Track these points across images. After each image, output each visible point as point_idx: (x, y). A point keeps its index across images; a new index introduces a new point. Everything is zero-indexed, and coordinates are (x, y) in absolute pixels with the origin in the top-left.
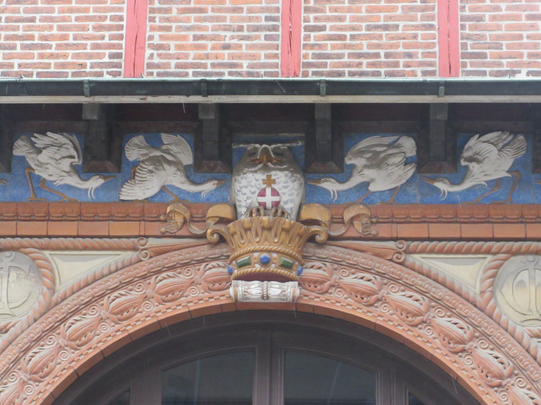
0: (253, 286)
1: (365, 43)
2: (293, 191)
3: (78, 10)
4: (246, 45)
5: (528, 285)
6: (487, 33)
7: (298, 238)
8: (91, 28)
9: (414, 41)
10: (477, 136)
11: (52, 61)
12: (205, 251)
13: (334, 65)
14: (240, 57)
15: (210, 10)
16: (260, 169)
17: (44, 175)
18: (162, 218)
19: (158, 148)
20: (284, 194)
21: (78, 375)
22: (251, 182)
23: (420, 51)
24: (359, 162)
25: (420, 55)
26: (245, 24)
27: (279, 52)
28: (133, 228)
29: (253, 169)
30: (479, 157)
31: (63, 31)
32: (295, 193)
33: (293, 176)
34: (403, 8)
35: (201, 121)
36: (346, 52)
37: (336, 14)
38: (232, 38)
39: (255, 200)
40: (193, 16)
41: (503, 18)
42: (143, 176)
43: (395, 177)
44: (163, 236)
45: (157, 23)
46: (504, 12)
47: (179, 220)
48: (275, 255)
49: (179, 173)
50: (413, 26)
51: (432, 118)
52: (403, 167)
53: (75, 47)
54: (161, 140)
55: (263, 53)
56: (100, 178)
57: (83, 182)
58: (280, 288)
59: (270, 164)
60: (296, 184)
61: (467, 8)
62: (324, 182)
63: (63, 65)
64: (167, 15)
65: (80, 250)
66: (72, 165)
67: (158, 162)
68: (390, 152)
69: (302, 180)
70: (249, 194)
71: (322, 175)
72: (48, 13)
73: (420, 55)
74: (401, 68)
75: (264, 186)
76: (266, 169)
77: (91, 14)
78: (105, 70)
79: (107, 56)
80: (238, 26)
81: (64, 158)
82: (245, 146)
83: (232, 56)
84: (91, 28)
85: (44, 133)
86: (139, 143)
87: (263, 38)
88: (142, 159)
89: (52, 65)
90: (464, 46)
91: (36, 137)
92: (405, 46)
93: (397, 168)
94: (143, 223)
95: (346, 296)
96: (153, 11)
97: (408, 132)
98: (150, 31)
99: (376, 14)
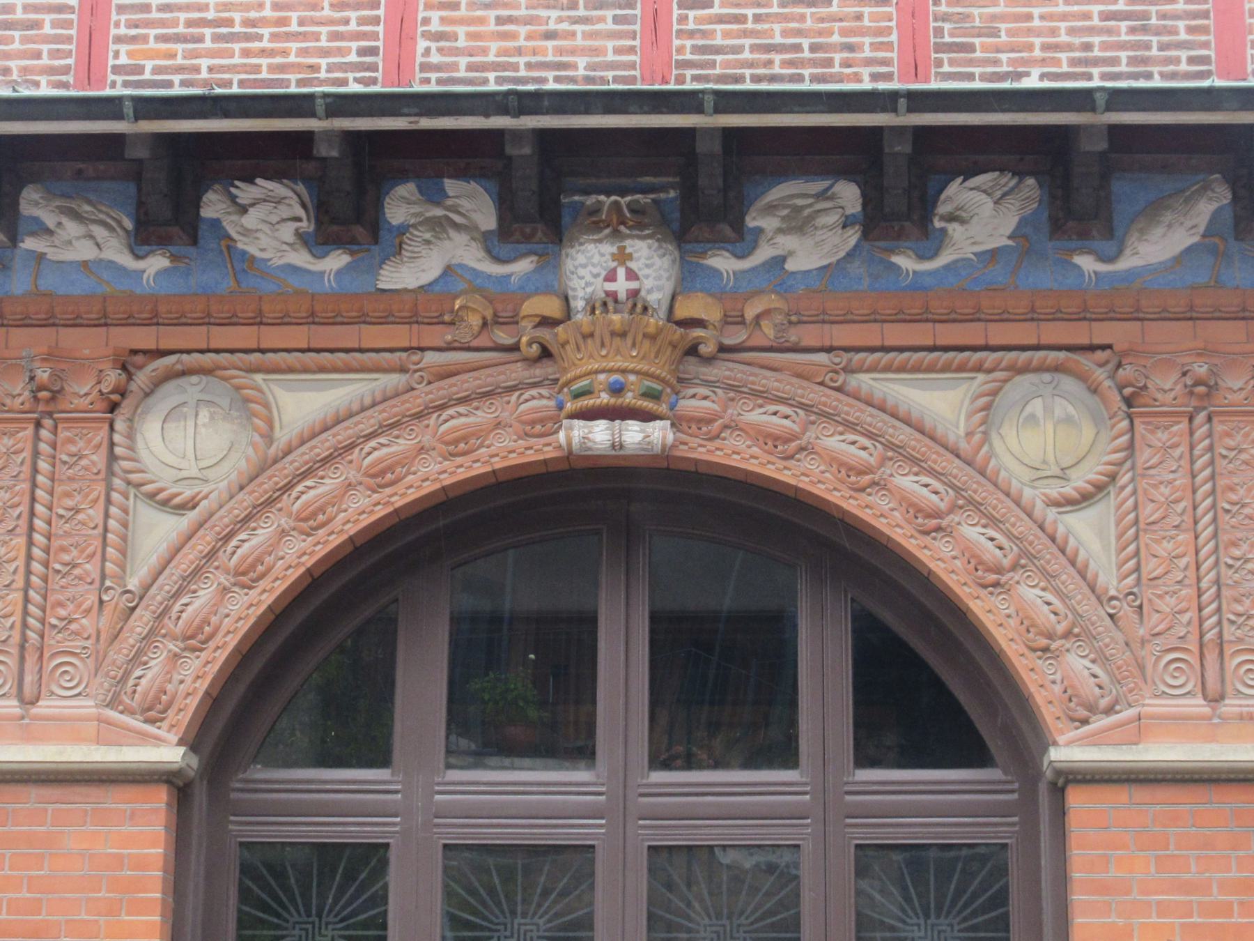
1: (777, 27)
2: (662, 272)
4: (584, 33)
5: (1042, 421)
7: (670, 349)
9: (858, 24)
10: (960, 179)
11: (264, 62)
12: (518, 372)
13: (726, 64)
14: (573, 52)
16: (607, 237)
17: (253, 250)
18: (447, 318)
19: (438, 204)
20: (647, 277)
21: (311, 575)
22: (592, 257)
23: (867, 40)
24: (769, 223)
25: (867, 48)
27: (637, 43)
28: (400, 335)
30: (964, 214)
31: (281, 11)
32: (665, 275)
33: (660, 247)
35: (510, 158)
36: (747, 42)
38: (560, 20)
39: (599, 287)
42: (416, 249)
44: (449, 348)
47: (475, 321)
48: (632, 378)
49: (474, 244)
52: (840, 231)
55: (610, 45)
56: (345, 253)
57: (316, 261)
58: (642, 431)
59: (622, 228)
60: (666, 261)
62: (711, 257)
63: (282, 68)
65: (314, 372)
66: (297, 233)
67: (440, 226)
69: (677, 253)
70: (589, 278)
73: (867, 48)
75: (615, 264)
76: (616, 235)
78: (351, 76)
81: (284, 220)
83: (560, 51)
85: (250, 180)
87: (610, 20)
88: (412, 221)
89: (264, 68)
90: (939, 32)
91: (237, 187)
92: (844, 32)
93: (830, 233)
94: (415, 326)
95: (749, 443)
97: (846, 173)
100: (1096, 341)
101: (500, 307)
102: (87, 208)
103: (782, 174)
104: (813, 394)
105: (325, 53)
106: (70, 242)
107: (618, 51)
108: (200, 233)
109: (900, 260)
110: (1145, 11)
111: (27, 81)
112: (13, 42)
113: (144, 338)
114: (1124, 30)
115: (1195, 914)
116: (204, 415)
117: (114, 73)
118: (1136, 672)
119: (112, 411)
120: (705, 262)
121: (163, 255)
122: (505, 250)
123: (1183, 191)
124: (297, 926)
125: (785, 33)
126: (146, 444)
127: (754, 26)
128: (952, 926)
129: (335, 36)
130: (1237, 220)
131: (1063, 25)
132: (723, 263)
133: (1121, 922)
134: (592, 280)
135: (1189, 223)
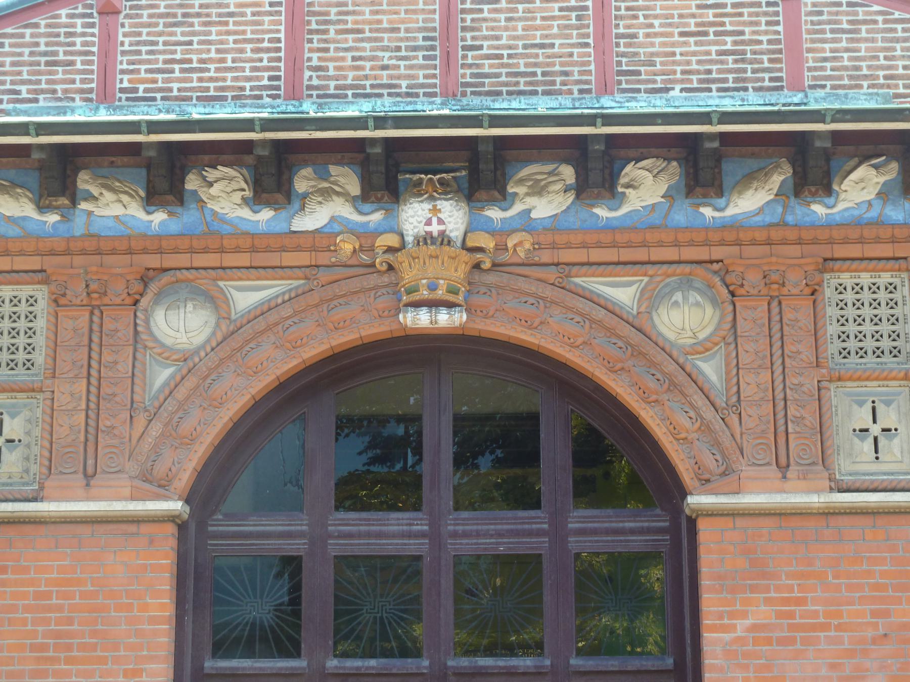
0: (422, 312)
1: (522, 62)
2: (458, 220)
3: (236, 33)
4: (405, 66)
5: (682, 305)
6: (641, 50)
7: (464, 265)
8: (249, 50)
9: (571, 59)
10: (633, 163)
11: (212, 85)
13: (492, 84)
14: (399, 77)
15: (367, 31)
16: (426, 199)
17: (216, 208)
18: (332, 248)
19: (326, 180)
20: (450, 223)
21: (254, 399)
22: (417, 211)
23: (576, 69)
24: (521, 190)
25: (576, 74)
26: (403, 44)
27: (437, 72)
29: (419, 200)
30: (635, 184)
31: (221, 54)
32: (460, 221)
33: (458, 205)
34: (558, 26)
35: (368, 154)
36: (504, 71)
37: (493, 33)
38: (391, 58)
39: (421, 229)
40: (350, 36)
41: (656, 35)
42: (314, 207)
43: (556, 203)
45: (315, 45)
46: (657, 30)
50: (568, 44)
51: (590, 148)
53: (234, 70)
54: (329, 171)
55: (421, 73)
56: (271, 209)
57: (254, 215)
59: (435, 194)
60: (461, 213)
61: (621, 26)
63: (222, 89)
64: (324, 37)
66: (243, 198)
67: (327, 194)
68: (551, 179)
69: (467, 208)
71: (485, 203)
72: (205, 36)
73: (576, 74)
74: (558, 87)
75: (430, 215)
76: (432, 198)
77: (249, 36)
78: (264, 93)
79: (266, 78)
80: (396, 47)
81: (234, 190)
82: (411, 176)
83: (391, 77)
84: (249, 50)
85: (214, 167)
86: (307, 175)
87: (421, 58)
88: (311, 190)
89: (212, 89)
90: (619, 63)
91: (206, 171)
92: (562, 64)
94: (313, 253)
96: (311, 32)
97: (567, 161)
98: (308, 52)
99: (532, 33)
100: (714, 258)
101: (363, 242)
102: (118, 184)
103: (529, 161)
104: (548, 292)
105: (249, 79)
106: (108, 204)
107: (425, 77)
108: (185, 198)
109: (597, 211)
110: (744, 50)
111: (67, 98)
112: (58, 74)
113: (153, 261)
114: (730, 61)
115: (772, 591)
116: (190, 306)
117: (120, 92)
118: (738, 452)
119: (135, 305)
120: (484, 213)
121: (163, 212)
122: (367, 207)
123: (764, 168)
124: (249, 604)
125: (526, 65)
126: (156, 323)
127: (508, 61)
128: (389, 602)
129: (254, 69)
130: (687, 185)
131: (694, 59)
132: (494, 214)
133: (729, 596)
134: (418, 225)
135: (767, 188)
